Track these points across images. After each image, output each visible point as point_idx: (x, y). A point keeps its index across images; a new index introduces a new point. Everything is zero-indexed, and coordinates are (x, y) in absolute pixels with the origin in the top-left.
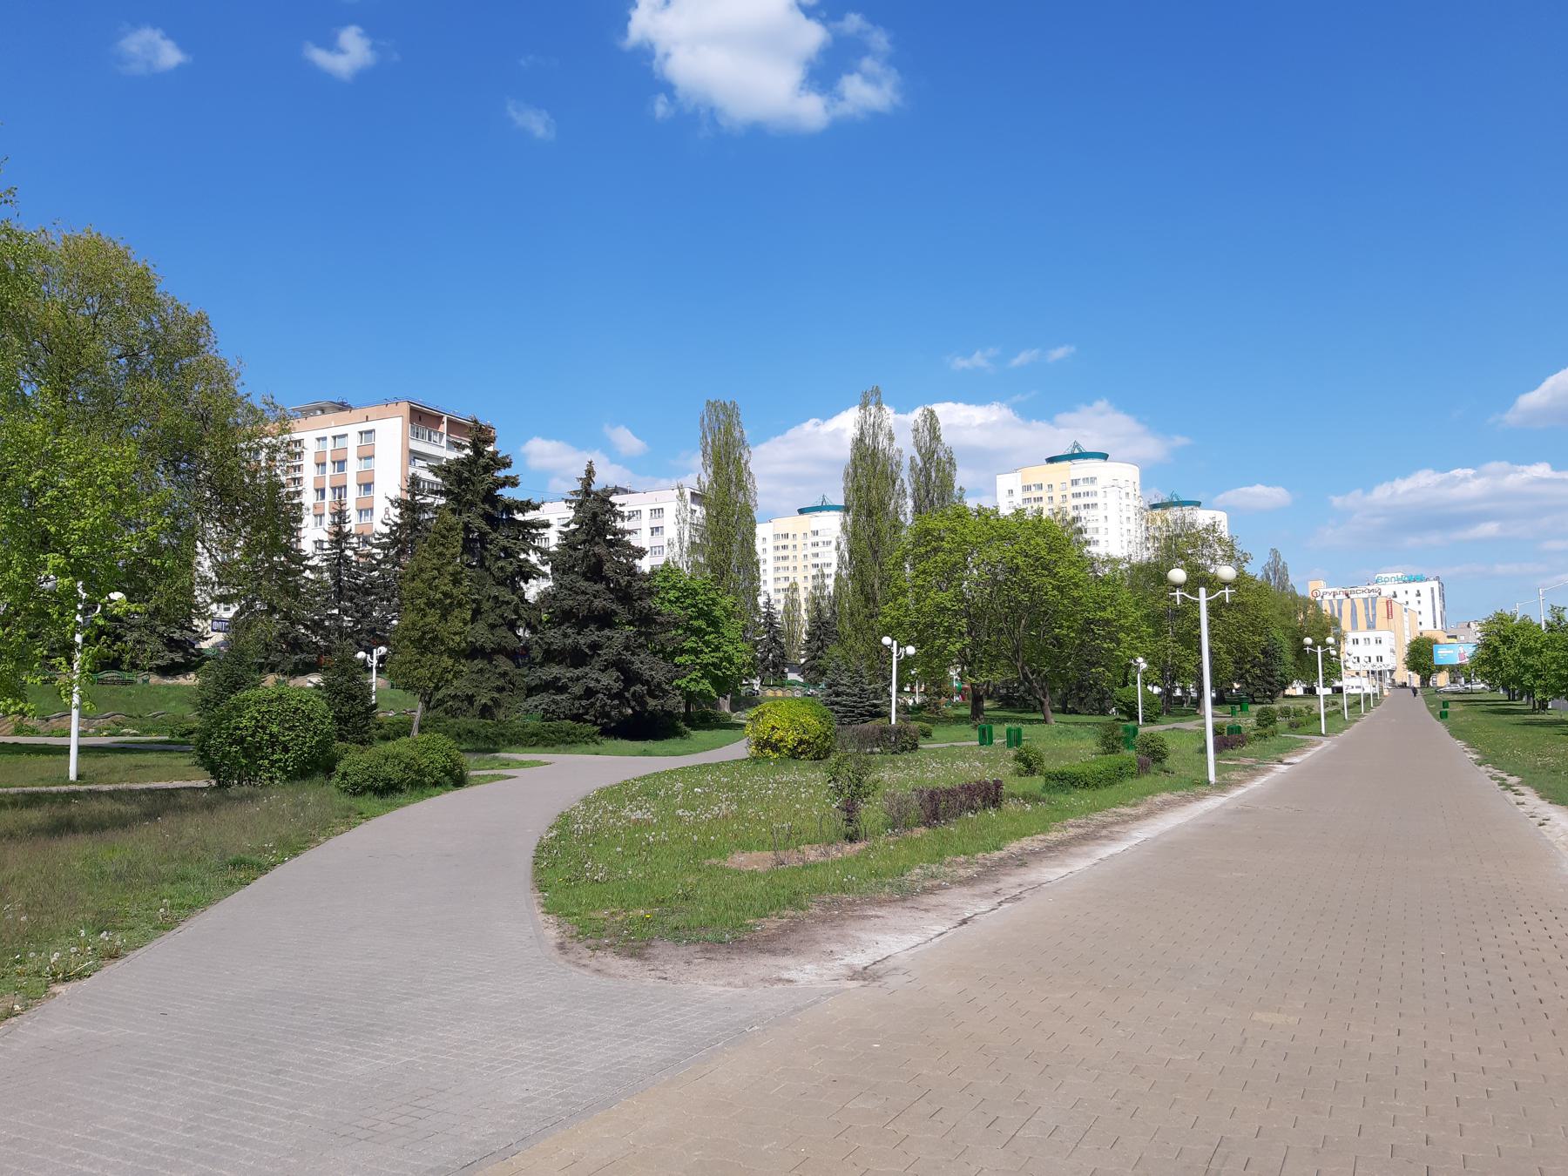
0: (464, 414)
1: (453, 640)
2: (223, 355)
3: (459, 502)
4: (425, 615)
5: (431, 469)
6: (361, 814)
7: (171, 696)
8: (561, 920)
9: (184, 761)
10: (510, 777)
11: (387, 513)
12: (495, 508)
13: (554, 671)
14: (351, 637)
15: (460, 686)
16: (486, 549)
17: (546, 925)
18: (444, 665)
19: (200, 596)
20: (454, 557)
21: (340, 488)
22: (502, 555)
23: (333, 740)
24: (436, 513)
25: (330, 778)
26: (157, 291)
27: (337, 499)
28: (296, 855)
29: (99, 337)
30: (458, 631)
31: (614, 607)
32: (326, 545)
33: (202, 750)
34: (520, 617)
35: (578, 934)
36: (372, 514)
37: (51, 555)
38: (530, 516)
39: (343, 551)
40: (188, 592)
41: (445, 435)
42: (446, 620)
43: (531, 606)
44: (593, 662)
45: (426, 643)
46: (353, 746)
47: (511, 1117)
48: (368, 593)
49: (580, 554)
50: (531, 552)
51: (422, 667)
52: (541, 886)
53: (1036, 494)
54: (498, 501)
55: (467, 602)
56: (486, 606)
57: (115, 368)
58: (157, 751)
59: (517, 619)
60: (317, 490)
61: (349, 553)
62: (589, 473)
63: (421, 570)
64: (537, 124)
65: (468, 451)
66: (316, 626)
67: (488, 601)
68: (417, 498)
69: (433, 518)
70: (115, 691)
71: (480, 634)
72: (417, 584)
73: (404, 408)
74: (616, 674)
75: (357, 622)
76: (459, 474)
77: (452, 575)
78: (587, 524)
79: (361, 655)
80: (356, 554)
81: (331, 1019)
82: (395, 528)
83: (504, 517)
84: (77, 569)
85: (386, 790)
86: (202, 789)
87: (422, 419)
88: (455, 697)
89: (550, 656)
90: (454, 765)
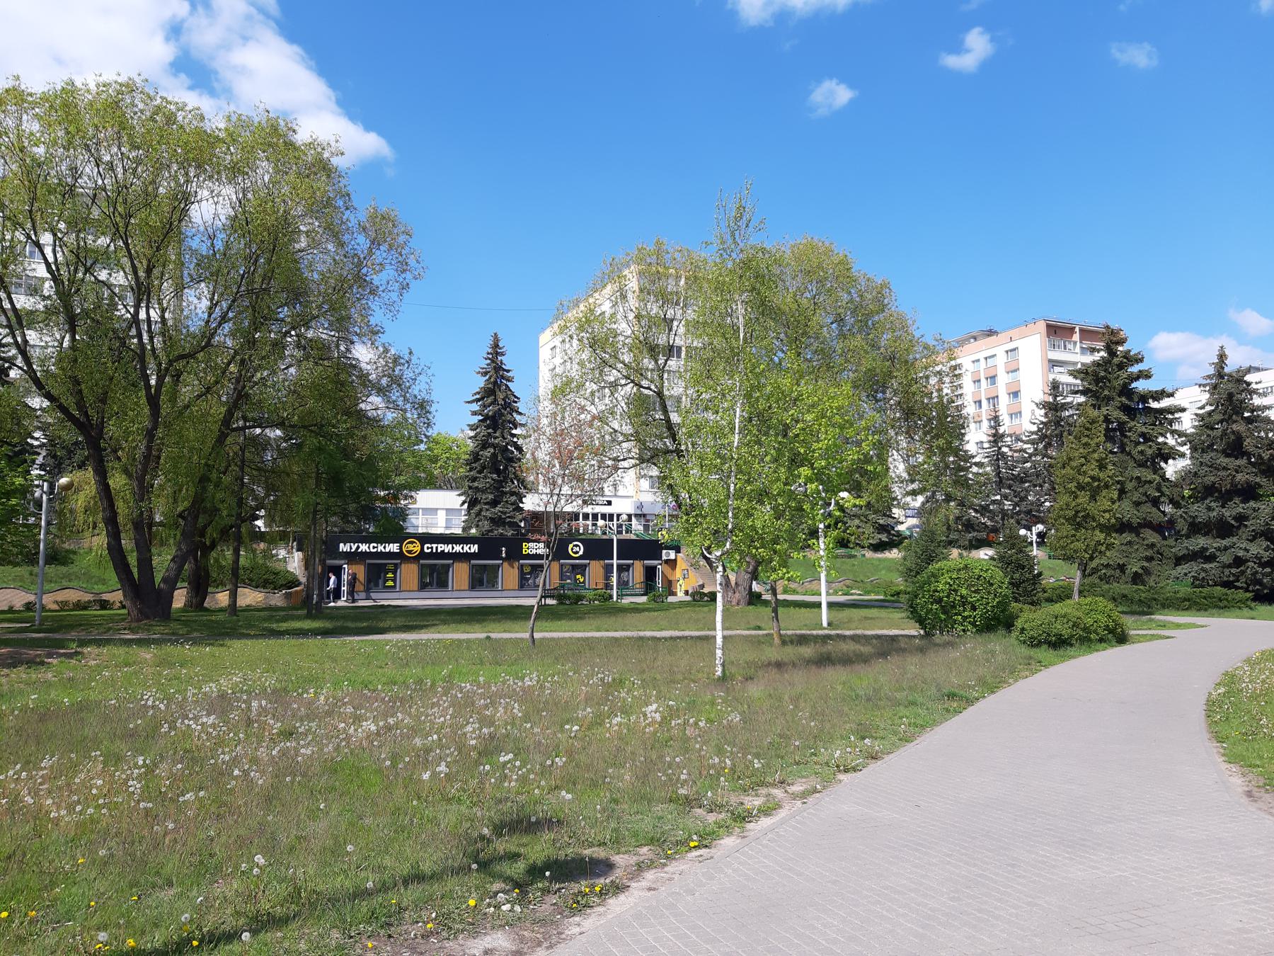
0: (1095, 321)
1: (1103, 517)
2: (901, 309)
3: (1097, 398)
4: (1076, 497)
5: (1071, 373)
6: (1040, 662)
7: (882, 566)
8: (1246, 770)
9: (897, 615)
10: (1168, 637)
11: (1033, 414)
12: (1130, 399)
13: (1201, 542)
14: (1012, 518)
15: (1113, 556)
16: (1126, 436)
17: (1230, 773)
18: (1096, 538)
19: (897, 491)
20: (1098, 445)
21: (993, 398)
22: (1141, 440)
23: (1010, 601)
24: (1077, 410)
25: (1010, 632)
26: (853, 270)
27: (992, 407)
28: (993, 692)
29: (818, 311)
30: (1107, 507)
31: (1258, 480)
32: (986, 445)
33: (912, 607)
34: (1163, 494)
35: (1265, 784)
36: (1021, 416)
37: (802, 469)
38: (1165, 403)
39: (1000, 448)
40: (887, 489)
41: (1078, 343)
42: (1095, 500)
43: (1172, 484)
44: (1240, 532)
45: (1080, 521)
46: (1026, 607)
47: (1230, 942)
48: (1022, 481)
49: (1217, 433)
50: (1168, 435)
51: (1078, 541)
52: (1219, 738)
54: (1133, 393)
55: (1113, 484)
56: (1129, 486)
57: (830, 332)
58: (877, 607)
59: (1161, 496)
60: (975, 402)
61: (1005, 450)
62: (1221, 356)
63: (1070, 459)
64: (1139, 57)
65: (1103, 354)
66: (983, 510)
67: (1131, 481)
68: (1058, 399)
69: (1073, 415)
70: (843, 562)
71: (1126, 510)
72: (1068, 470)
73: (1042, 326)
74: (1265, 544)
75: (1016, 505)
76: (1095, 374)
77: (1097, 461)
78: (1222, 405)
79: (1023, 532)
80: (1011, 450)
81: (1048, 829)
82: (1041, 426)
83: (1140, 407)
84: (818, 477)
85: (1059, 643)
86: (914, 636)
87: (1057, 332)
88: (1108, 566)
89: (1196, 528)
90: (1116, 625)
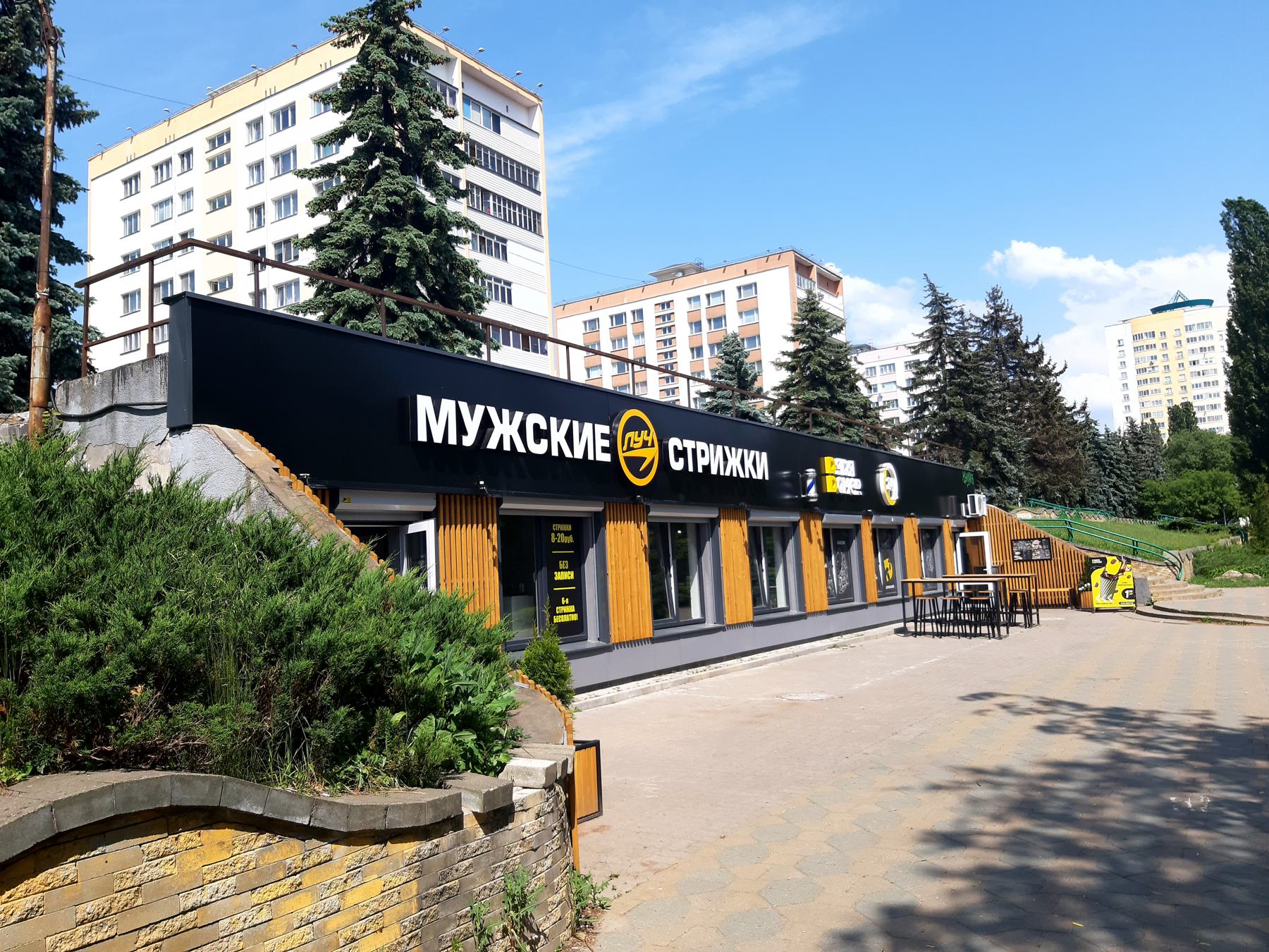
53: (1147, 341)
73: (790, 259)
